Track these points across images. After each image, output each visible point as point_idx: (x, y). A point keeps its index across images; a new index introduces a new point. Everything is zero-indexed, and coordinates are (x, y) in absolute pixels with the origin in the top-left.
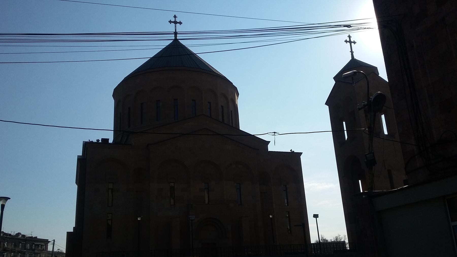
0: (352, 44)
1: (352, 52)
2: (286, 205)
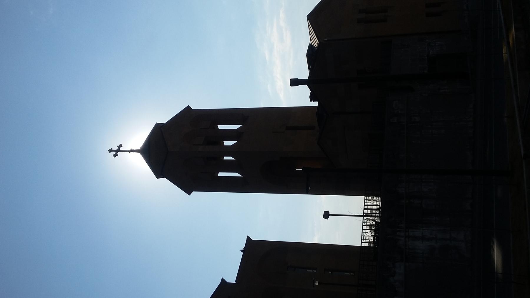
0: (121, 149)
1: (131, 151)
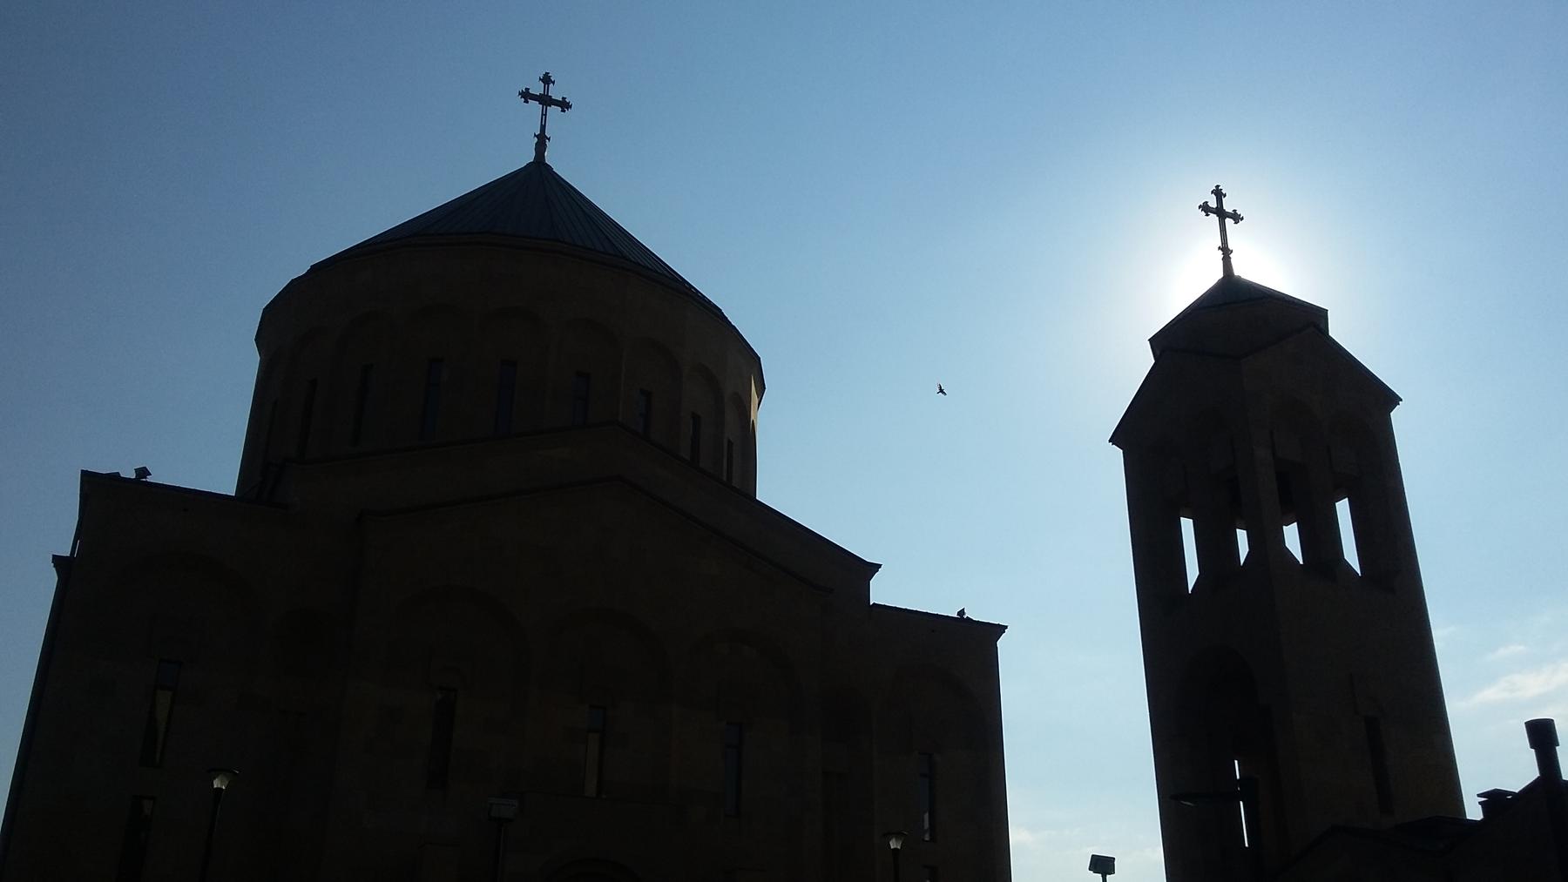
0: (1229, 222)
1: (1226, 251)
2: (927, 839)
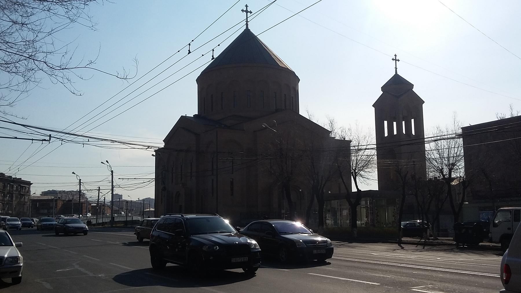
0: (397, 61)
1: (396, 68)
